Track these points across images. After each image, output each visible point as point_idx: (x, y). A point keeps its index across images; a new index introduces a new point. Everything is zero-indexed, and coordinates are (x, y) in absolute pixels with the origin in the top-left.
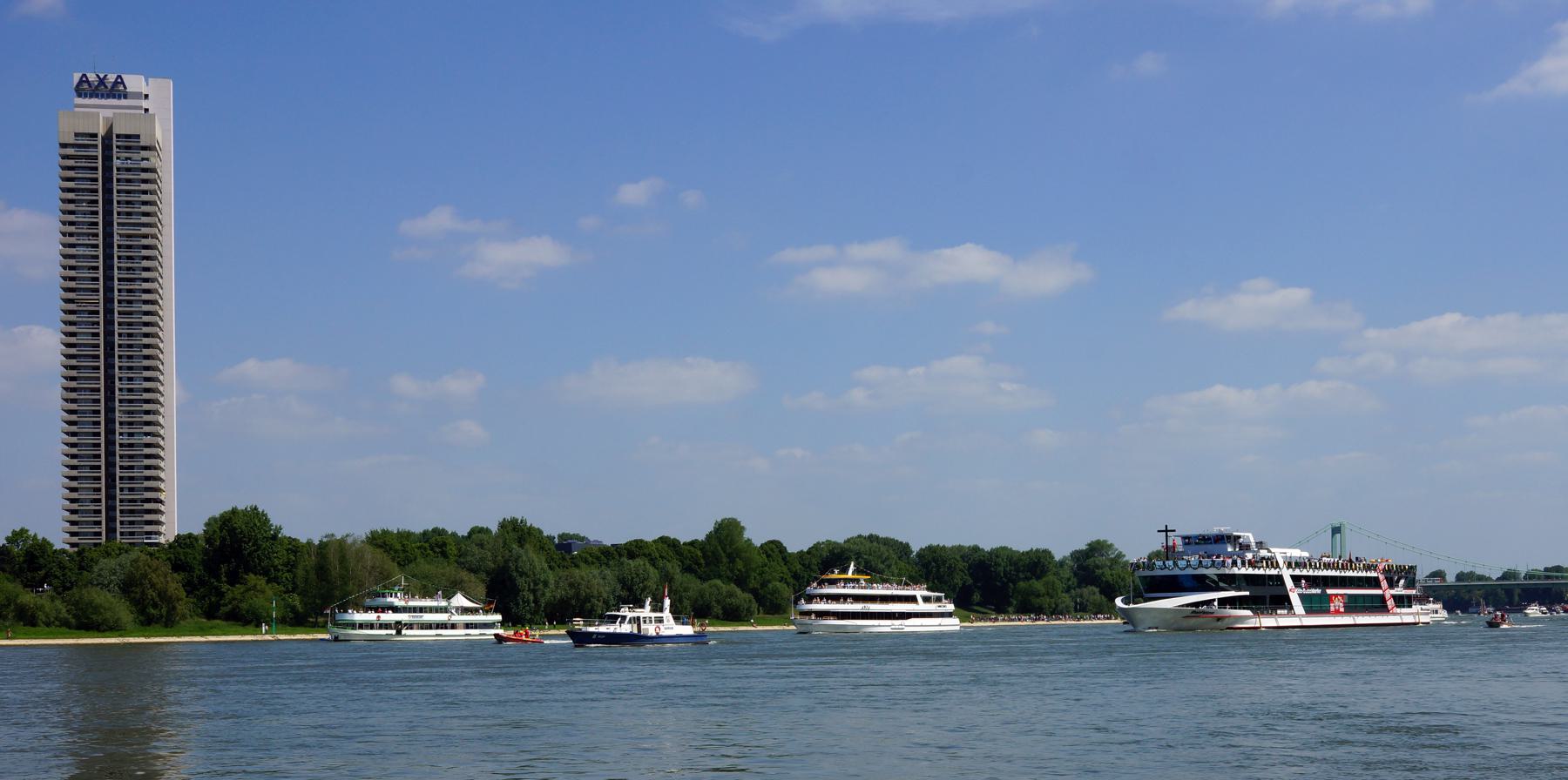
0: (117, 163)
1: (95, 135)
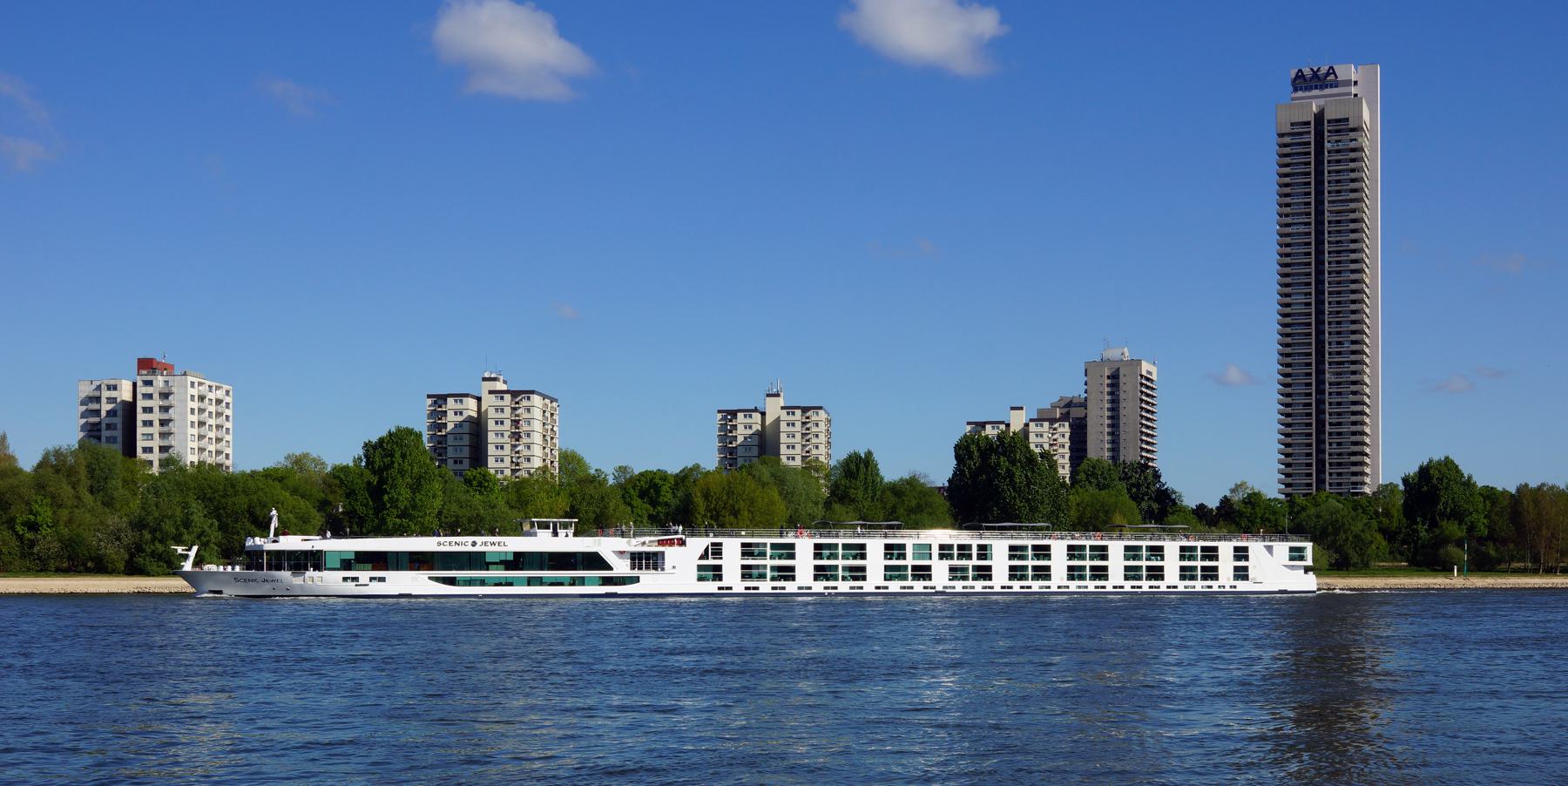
0: (1327, 145)
1: (1308, 123)
